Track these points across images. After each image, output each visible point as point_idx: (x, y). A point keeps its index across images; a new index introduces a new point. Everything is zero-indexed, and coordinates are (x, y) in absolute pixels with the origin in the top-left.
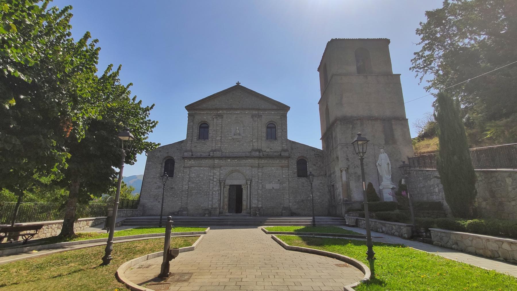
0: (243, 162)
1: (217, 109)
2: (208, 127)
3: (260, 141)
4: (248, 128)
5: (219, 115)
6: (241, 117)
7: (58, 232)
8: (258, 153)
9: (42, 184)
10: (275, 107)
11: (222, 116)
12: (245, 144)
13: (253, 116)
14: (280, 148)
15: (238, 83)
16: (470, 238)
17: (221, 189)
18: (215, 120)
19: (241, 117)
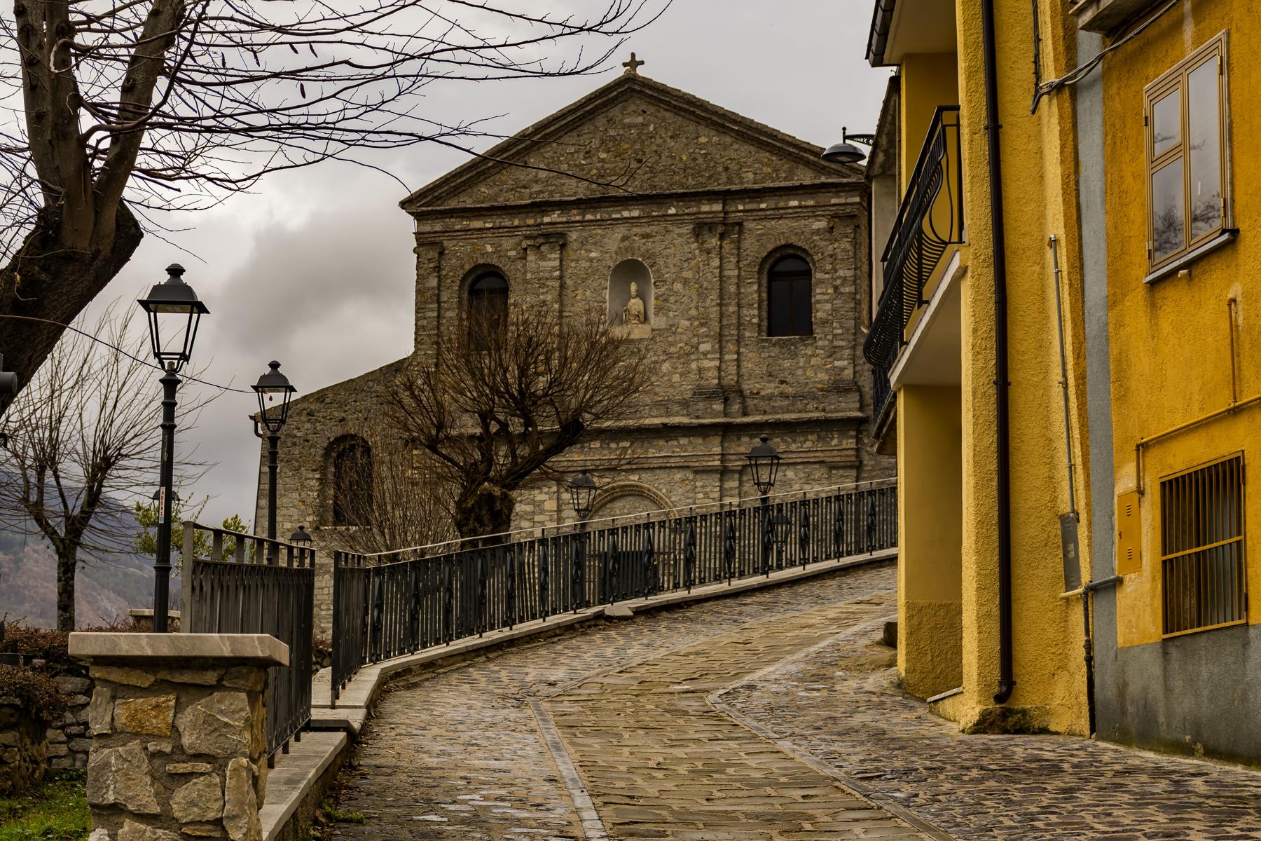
0: (656, 451)
1: (542, 207)
2: (505, 291)
3: (731, 347)
4: (678, 286)
5: (547, 236)
6: (646, 236)
7: (147, 685)
8: (718, 407)
9: (125, 598)
10: (805, 177)
11: (562, 235)
12: (666, 367)
13: (701, 228)
14: (823, 376)
15: (634, 63)
16: (428, 617)
17: (91, 630)
18: (531, 257)
19: (646, 236)
